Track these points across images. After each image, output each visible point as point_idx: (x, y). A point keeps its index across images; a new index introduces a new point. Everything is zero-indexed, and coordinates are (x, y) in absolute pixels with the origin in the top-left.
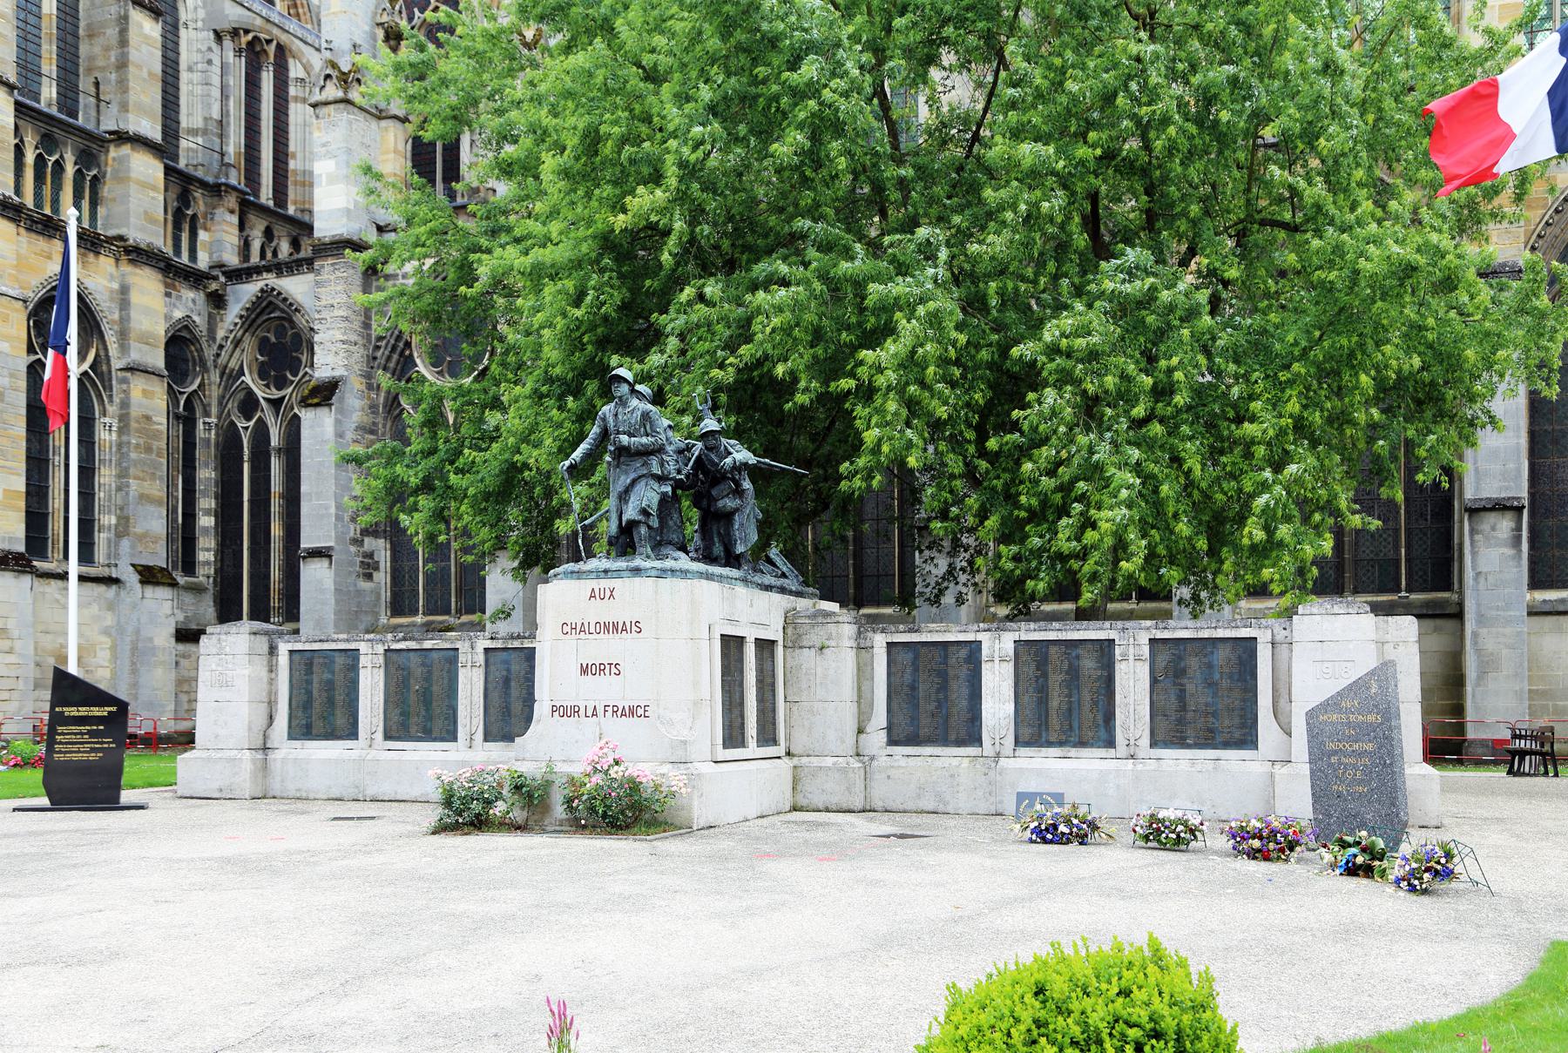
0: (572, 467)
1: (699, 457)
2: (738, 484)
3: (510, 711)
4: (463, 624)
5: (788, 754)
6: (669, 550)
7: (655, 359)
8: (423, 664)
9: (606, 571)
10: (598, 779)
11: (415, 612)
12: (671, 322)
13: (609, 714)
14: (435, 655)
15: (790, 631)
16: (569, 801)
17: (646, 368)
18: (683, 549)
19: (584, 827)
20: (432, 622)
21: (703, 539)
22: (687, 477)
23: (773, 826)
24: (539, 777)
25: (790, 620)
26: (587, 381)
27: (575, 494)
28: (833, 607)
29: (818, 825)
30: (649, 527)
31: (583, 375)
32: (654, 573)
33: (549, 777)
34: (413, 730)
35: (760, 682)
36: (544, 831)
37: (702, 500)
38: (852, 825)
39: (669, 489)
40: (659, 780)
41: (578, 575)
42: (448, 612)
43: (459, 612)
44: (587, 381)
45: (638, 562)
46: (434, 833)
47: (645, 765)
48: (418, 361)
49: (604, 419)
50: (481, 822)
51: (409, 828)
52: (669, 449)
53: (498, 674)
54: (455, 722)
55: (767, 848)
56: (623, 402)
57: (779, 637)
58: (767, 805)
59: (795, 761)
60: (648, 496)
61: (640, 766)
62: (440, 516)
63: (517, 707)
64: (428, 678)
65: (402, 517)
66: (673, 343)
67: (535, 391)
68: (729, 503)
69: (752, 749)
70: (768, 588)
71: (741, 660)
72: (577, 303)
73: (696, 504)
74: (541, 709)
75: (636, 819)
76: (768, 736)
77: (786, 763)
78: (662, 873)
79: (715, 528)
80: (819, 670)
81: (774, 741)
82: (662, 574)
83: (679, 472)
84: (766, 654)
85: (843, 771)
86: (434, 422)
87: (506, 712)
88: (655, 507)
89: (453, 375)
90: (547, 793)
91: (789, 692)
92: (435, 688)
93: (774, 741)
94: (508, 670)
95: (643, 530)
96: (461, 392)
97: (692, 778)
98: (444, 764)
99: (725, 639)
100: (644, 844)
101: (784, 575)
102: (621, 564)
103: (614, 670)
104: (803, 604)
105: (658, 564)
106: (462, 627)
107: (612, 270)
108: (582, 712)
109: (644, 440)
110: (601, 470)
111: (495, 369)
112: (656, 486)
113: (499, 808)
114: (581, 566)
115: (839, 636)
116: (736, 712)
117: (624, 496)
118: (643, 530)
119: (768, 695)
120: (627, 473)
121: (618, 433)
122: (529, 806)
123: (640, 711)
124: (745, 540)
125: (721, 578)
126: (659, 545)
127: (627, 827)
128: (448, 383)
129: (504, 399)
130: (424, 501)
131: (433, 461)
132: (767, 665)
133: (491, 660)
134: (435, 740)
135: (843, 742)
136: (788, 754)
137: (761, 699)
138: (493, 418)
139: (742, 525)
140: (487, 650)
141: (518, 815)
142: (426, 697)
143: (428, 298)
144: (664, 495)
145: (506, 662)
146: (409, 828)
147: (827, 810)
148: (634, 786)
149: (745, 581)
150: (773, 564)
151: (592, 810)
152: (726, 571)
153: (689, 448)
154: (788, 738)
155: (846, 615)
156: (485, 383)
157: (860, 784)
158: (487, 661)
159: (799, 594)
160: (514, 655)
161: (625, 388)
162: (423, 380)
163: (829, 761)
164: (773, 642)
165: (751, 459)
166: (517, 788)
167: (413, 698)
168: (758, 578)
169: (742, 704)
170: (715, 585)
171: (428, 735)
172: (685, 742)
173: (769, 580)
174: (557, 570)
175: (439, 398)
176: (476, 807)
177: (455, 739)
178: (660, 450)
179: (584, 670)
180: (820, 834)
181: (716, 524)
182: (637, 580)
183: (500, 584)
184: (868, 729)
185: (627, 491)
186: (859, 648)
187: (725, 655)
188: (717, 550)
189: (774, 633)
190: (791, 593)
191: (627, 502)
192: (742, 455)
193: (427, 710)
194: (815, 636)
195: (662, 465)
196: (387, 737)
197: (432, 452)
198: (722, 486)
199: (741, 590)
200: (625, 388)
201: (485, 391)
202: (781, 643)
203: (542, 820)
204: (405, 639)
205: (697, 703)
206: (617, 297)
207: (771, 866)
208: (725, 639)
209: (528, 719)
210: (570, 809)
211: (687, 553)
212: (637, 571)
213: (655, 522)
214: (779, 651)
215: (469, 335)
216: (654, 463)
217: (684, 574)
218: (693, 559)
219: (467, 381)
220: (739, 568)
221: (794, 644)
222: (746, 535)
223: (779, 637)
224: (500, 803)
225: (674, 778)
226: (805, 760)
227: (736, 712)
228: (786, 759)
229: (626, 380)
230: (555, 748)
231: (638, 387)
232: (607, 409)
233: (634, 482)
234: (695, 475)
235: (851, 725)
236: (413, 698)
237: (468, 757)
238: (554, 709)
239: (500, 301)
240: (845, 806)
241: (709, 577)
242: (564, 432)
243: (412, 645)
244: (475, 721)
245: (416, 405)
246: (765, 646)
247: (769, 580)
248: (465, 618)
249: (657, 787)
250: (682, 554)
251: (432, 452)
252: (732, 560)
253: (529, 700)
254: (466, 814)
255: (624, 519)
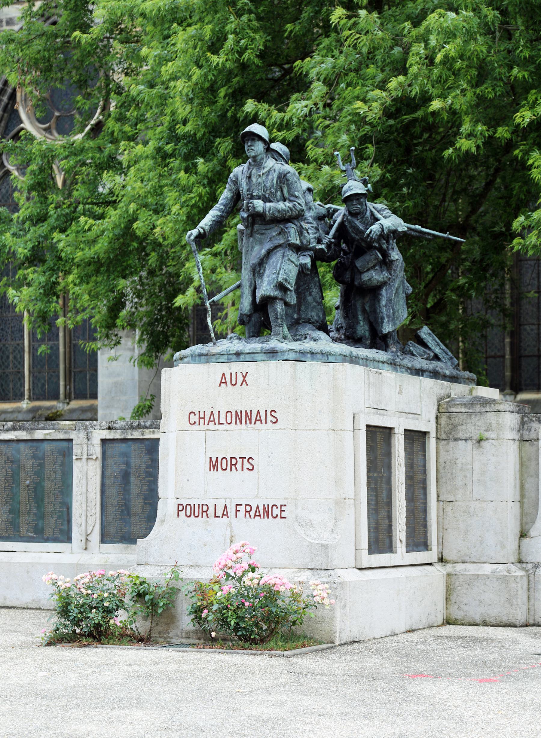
0: (200, 236)
1: (342, 224)
2: (385, 254)
3: (131, 508)
4: (72, 411)
5: (441, 560)
6: (307, 330)
7: (298, 107)
8: (34, 457)
9: (238, 354)
10: (230, 587)
11: (19, 397)
12: (317, 66)
13: (241, 514)
14: (47, 446)
15: (443, 420)
16: (197, 611)
17: (287, 117)
18: (323, 328)
19: (214, 640)
20: (39, 408)
21: (346, 316)
22: (329, 246)
23: (424, 641)
24: (163, 583)
25: (444, 408)
26: (221, 136)
27: (198, 267)
28: (492, 393)
29: (475, 641)
30: (286, 304)
31: (214, 131)
32: (292, 356)
33: (174, 584)
34: (24, 529)
35: (410, 478)
36: (169, 644)
37: (346, 275)
38: (515, 642)
39: (307, 261)
40: (298, 589)
41: (207, 358)
42: (55, 397)
43: (68, 397)
44: (221, 136)
45: (274, 343)
46: (49, 644)
47: (281, 567)
48: (23, 115)
49: (236, 182)
50: (100, 633)
51: (22, 638)
52: (309, 215)
53: (115, 469)
54: (69, 521)
55: (418, 667)
56: (257, 163)
57: (430, 427)
58: (418, 617)
59: (449, 568)
60: (285, 268)
61: (277, 572)
62: (50, 290)
63: (137, 505)
64: (39, 472)
65: (11, 292)
66: (318, 89)
67: (159, 150)
68: (375, 276)
69: (401, 554)
70: (419, 372)
71: (388, 454)
72: (215, 47)
73: (338, 277)
74: (166, 507)
75: (272, 632)
76: (418, 540)
77: (439, 571)
78: (303, 693)
79: (359, 305)
80: (477, 466)
81: (426, 546)
82: (301, 357)
83: (319, 241)
84: (417, 447)
85: (504, 580)
86: (42, 186)
87: (125, 510)
88: (293, 281)
89: (62, 131)
90: (172, 602)
91: (443, 490)
92: (47, 483)
93: (426, 546)
94: (127, 464)
95: (279, 307)
96: (74, 151)
97: (337, 588)
98: (58, 567)
99: (373, 431)
100: (282, 661)
101: (436, 358)
102: (255, 345)
103: (247, 465)
104: (458, 390)
105: (296, 346)
106: (71, 416)
107: (250, 12)
108: (211, 512)
109: (281, 205)
110: (228, 238)
111: (111, 125)
112: (294, 257)
113: (120, 618)
114: (209, 348)
115: (500, 427)
116: (383, 513)
117: (258, 269)
118: (279, 307)
119: (419, 493)
120: (261, 243)
121: (252, 197)
122: (151, 616)
123: (276, 511)
124: (393, 319)
125: (366, 362)
126: (296, 324)
127: (262, 641)
128: (58, 141)
129: (124, 158)
130: (36, 275)
131: (43, 229)
132: (418, 460)
133: (109, 453)
134: (47, 540)
135: (503, 547)
136: (441, 560)
137: (410, 499)
138: (109, 182)
139: (389, 300)
140: (104, 441)
141: (141, 626)
142: (37, 493)
143: (38, 45)
144: (302, 268)
145: (125, 455)
146: (22, 638)
147: (485, 624)
148: (271, 595)
149: (393, 364)
150: (424, 345)
151: (224, 622)
152: (372, 353)
153: (330, 214)
154: (441, 542)
155: (507, 404)
156: (99, 141)
157: (522, 595)
158: (104, 453)
159: (454, 379)
160: (134, 447)
161: (259, 147)
162: (31, 139)
163: (488, 569)
164: (424, 434)
165: (402, 226)
166: (140, 596)
167: (23, 493)
168: (407, 361)
169: (389, 504)
170: (359, 369)
171: (39, 535)
172: (326, 547)
173: (420, 363)
174: (183, 352)
175: (49, 157)
176: (95, 616)
177: (69, 540)
178: (296, 217)
179: (214, 465)
180: (478, 652)
181: (360, 297)
182: (273, 364)
183: (117, 365)
184: (532, 533)
185: (262, 263)
186: (523, 440)
187: (371, 448)
188: (361, 328)
189: (426, 423)
190: (445, 377)
191: (261, 275)
192: (390, 221)
193: (38, 507)
194: (472, 428)
195: (301, 234)
196: (104, 539)
197: (42, 218)
198: (367, 257)
199: (389, 375)
200: (259, 147)
201: (100, 149)
202: (433, 434)
203: (167, 631)
204: (14, 429)
205: (340, 502)
206: (260, 40)
207: (427, 688)
208: (373, 431)
209: (151, 518)
210: (198, 619)
211: (327, 332)
212: (272, 354)
213: (292, 299)
214: (432, 443)
215: (82, 84)
216: (292, 229)
217: (325, 357)
218: (335, 340)
219: (79, 137)
220: (386, 348)
221: (448, 435)
222: (395, 312)
223: (430, 427)
224: (121, 612)
225: (317, 587)
226: (459, 567)
227: (383, 513)
228: (438, 567)
229: (260, 138)
230: (182, 551)
231: (274, 146)
232: (239, 171)
233: (269, 253)
234: (337, 244)
235: (512, 528)
236: (23, 493)
237: (84, 560)
238: (180, 508)
239: (117, 46)
240: (505, 619)
241: (354, 360)
242: (193, 197)
243: (22, 435)
244: (91, 520)
245: (22, 169)
246: (416, 438)
247: (420, 363)
248: (75, 404)
249: (295, 597)
250: (322, 335)
251: (42, 218)
252: (378, 341)
253: (151, 498)
254: (85, 624)
255: (259, 295)
